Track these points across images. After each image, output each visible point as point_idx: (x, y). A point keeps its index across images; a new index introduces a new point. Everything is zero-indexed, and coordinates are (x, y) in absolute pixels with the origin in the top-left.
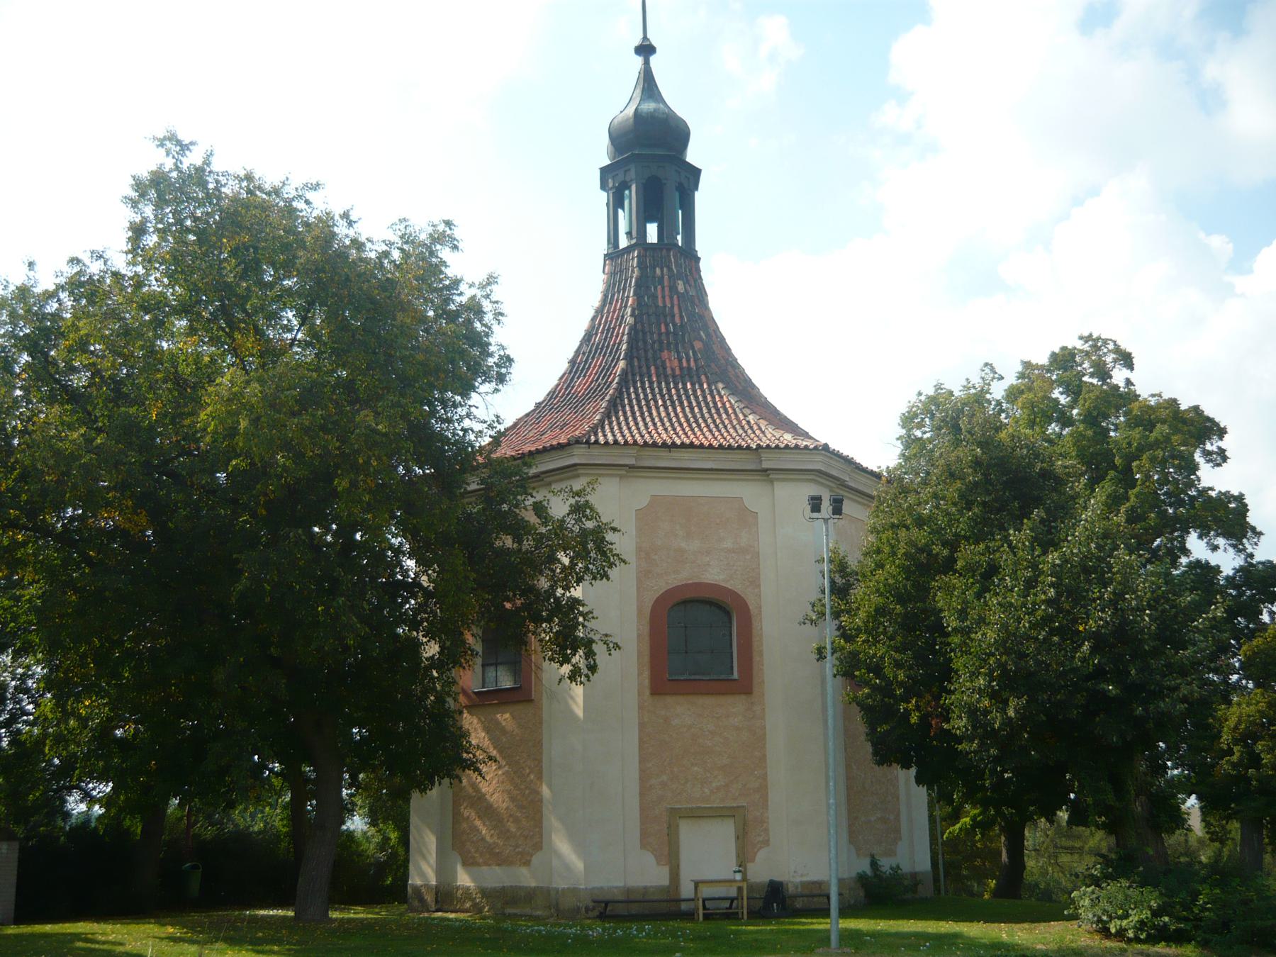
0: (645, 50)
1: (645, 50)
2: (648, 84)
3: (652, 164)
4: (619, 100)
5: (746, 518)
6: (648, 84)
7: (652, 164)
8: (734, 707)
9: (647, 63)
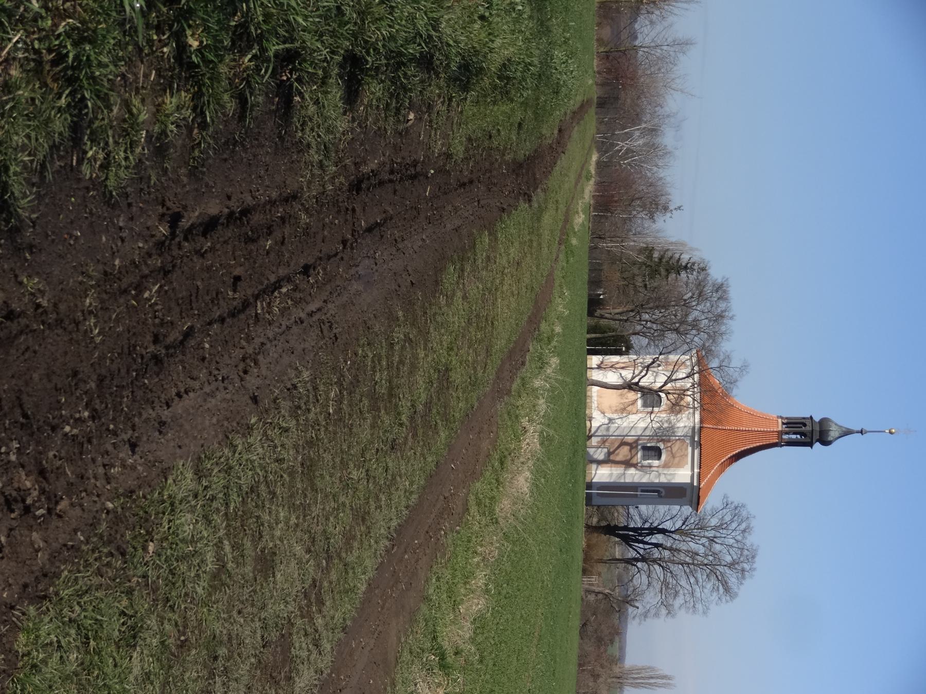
2: (848, 432)
4: (839, 418)
6: (848, 432)
9: (858, 432)
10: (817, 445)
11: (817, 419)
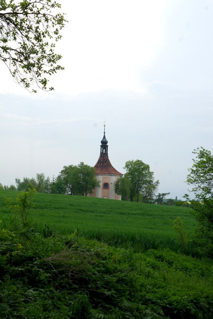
0: (104, 133)
1: (104, 133)
2: (104, 137)
3: (104, 144)
5: (109, 178)
6: (104, 137)
7: (104, 144)
8: (108, 190)
10: (108, 144)
11: (101, 144)
